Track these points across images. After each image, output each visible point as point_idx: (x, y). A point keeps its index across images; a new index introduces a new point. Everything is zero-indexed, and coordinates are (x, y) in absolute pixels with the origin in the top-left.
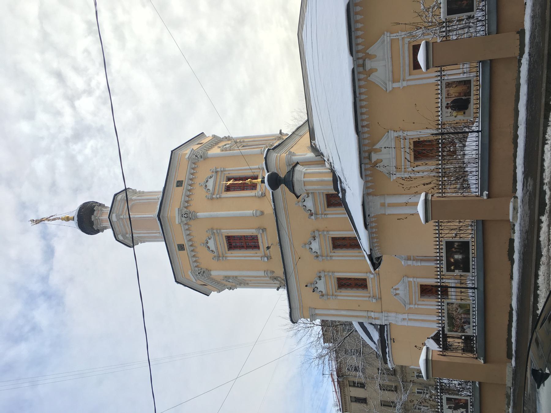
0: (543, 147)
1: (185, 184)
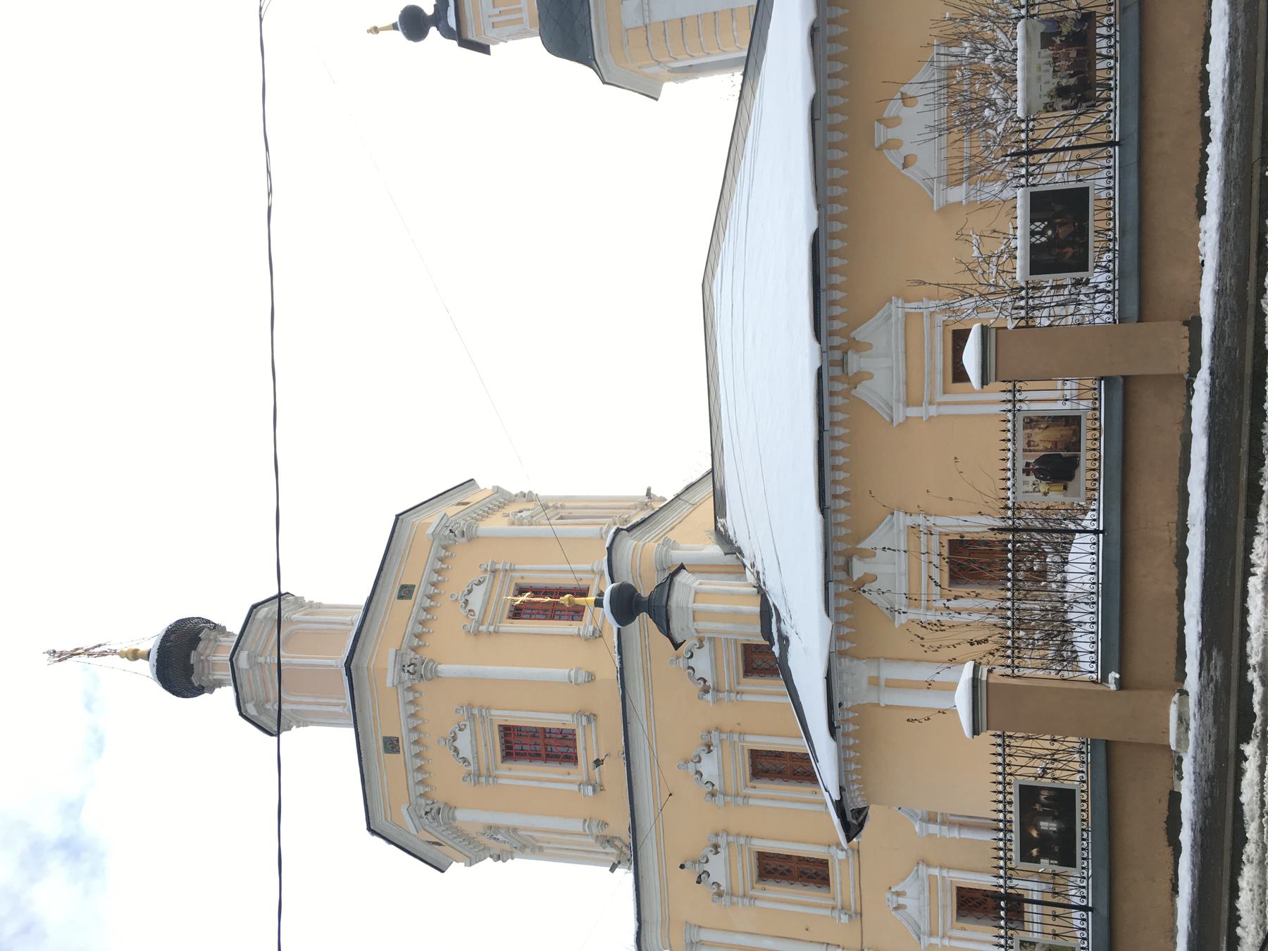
1: (418, 594)
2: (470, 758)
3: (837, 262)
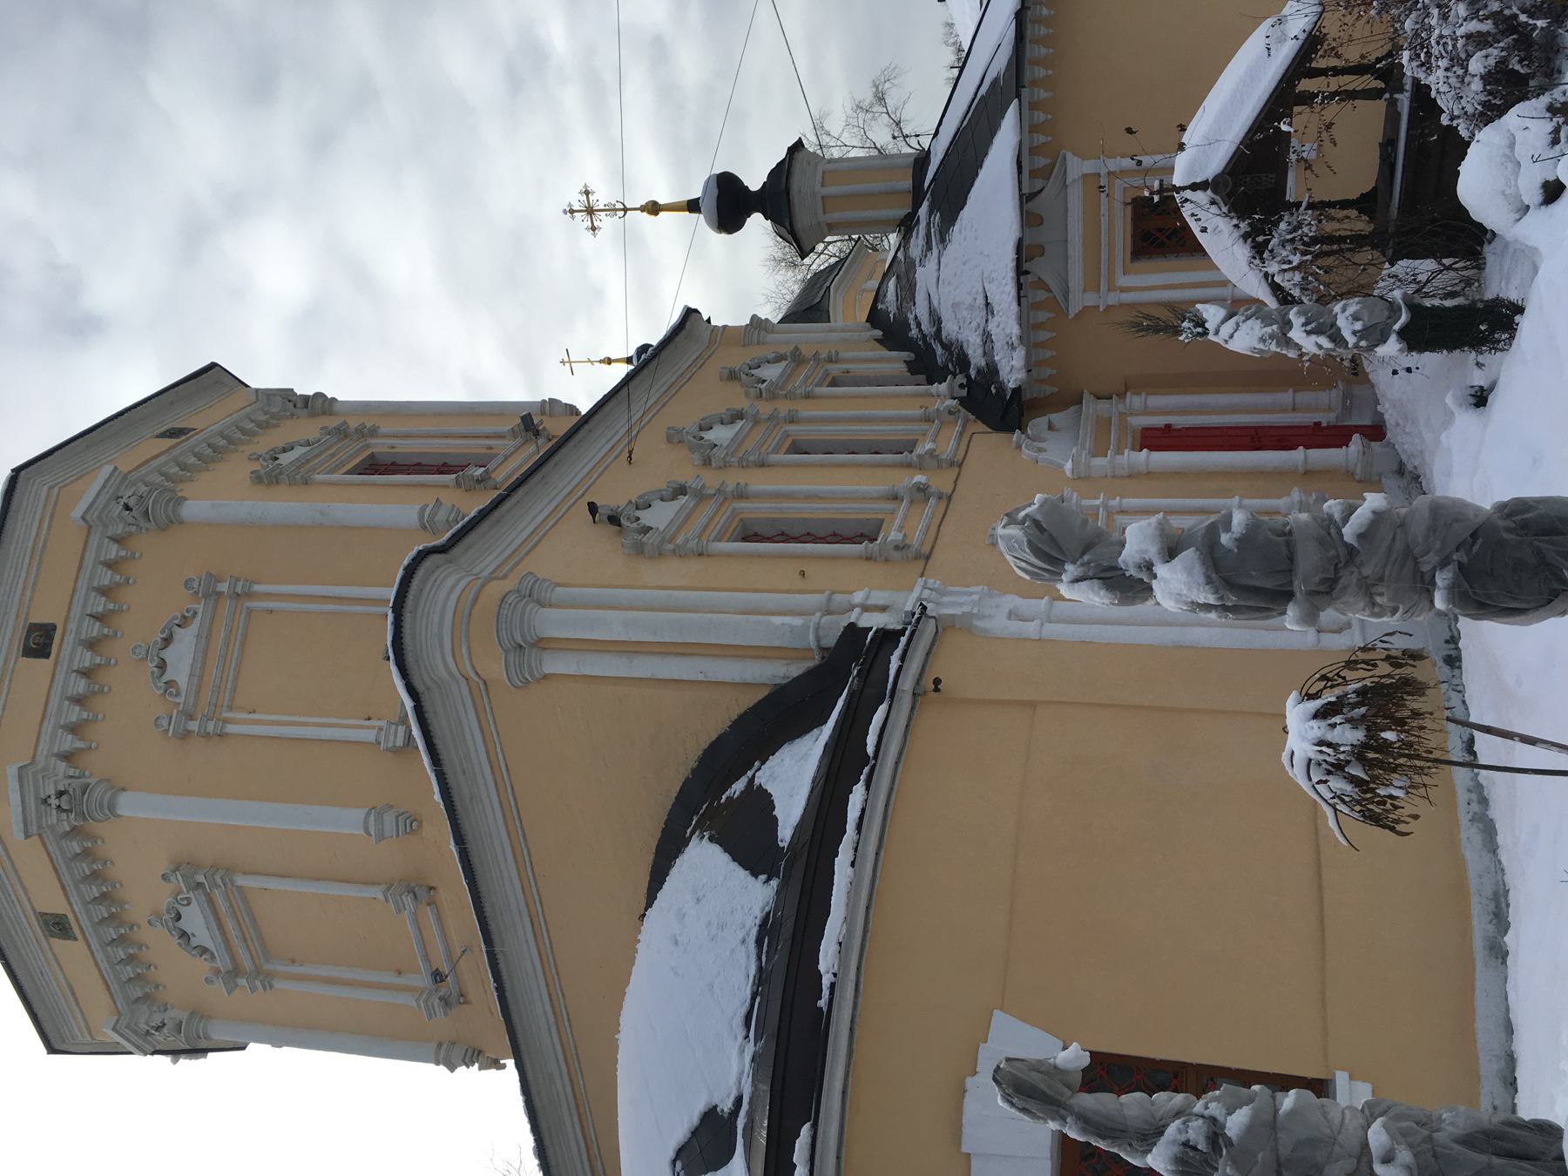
0: (850, 933)
1: (64, 645)
2: (210, 945)
3: (1041, 72)
